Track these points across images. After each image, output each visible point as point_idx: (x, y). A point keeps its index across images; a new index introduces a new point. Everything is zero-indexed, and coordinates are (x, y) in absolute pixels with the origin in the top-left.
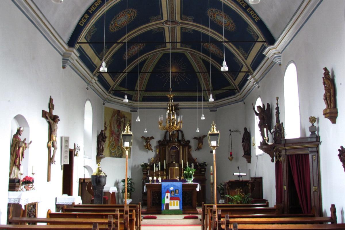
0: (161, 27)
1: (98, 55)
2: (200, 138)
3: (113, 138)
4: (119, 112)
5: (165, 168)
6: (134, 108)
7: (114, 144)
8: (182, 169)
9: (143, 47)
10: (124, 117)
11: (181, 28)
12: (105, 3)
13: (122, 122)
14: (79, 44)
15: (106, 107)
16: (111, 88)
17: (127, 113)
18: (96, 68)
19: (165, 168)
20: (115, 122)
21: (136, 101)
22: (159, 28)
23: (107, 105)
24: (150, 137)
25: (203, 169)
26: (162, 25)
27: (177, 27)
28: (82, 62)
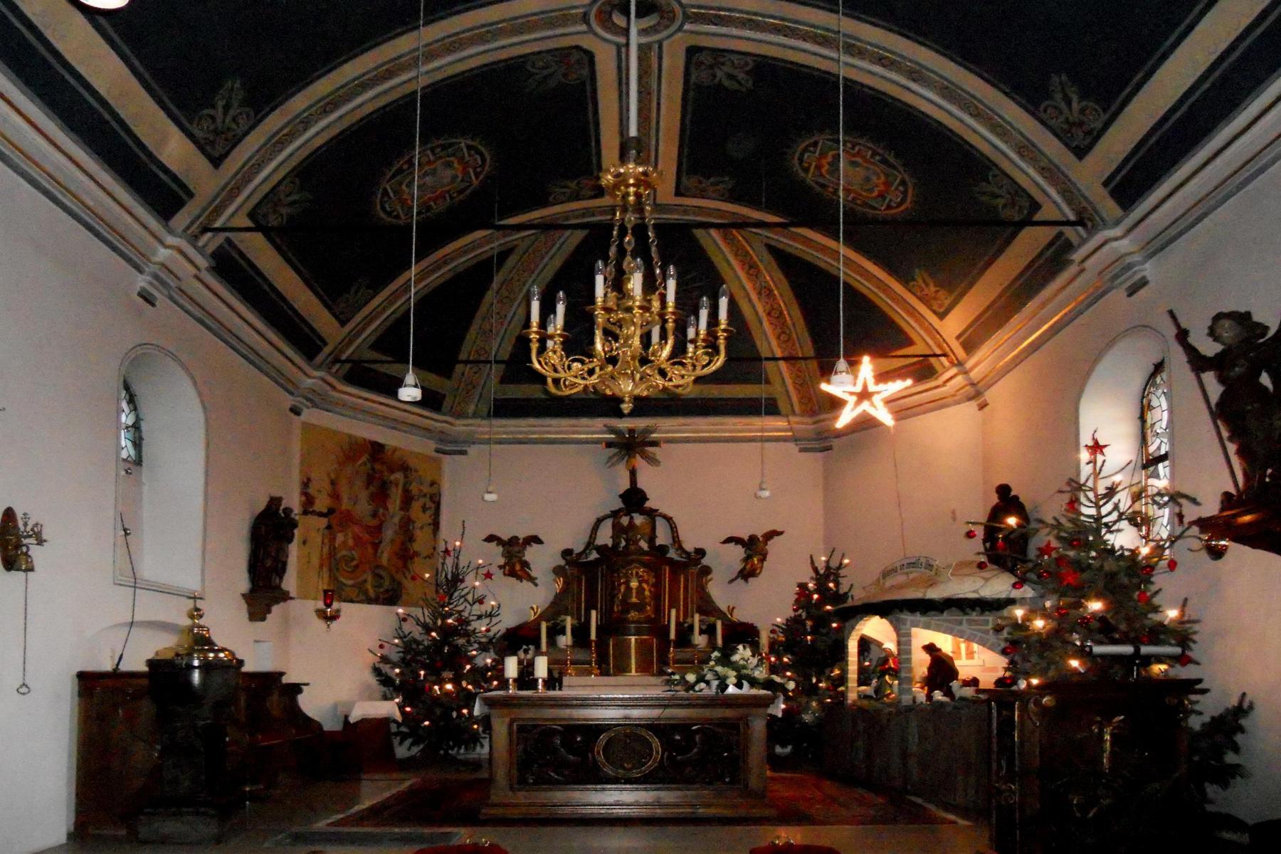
0: (578, 48)
1: (187, 125)
2: (753, 539)
3: (346, 536)
4: (376, 449)
5: (593, 636)
6: (456, 442)
7: (353, 559)
8: (669, 641)
9: (481, 177)
10: (405, 468)
11: (692, 51)
12: (410, 267)
13: (397, 485)
14: (223, 235)
15: (306, 426)
16: (327, 350)
17: (417, 455)
18: (184, 197)
19: (593, 636)
20: (359, 483)
21: (461, 415)
22: (563, 55)
23: (311, 415)
24: (522, 536)
25: (466, 689)
26: (584, 27)
27: (665, 44)
28: (149, 212)
